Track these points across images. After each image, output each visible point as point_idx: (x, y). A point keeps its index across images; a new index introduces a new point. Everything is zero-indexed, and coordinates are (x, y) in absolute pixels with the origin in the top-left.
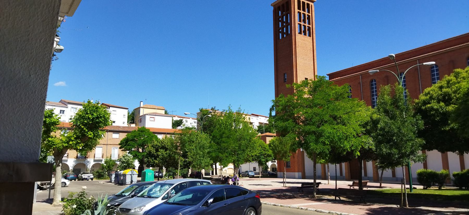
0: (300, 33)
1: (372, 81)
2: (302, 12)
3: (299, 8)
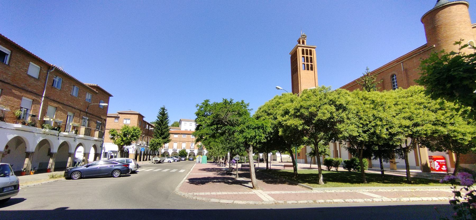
0: (242, 165)
1: (393, 76)
2: (305, 56)
3: (303, 53)
